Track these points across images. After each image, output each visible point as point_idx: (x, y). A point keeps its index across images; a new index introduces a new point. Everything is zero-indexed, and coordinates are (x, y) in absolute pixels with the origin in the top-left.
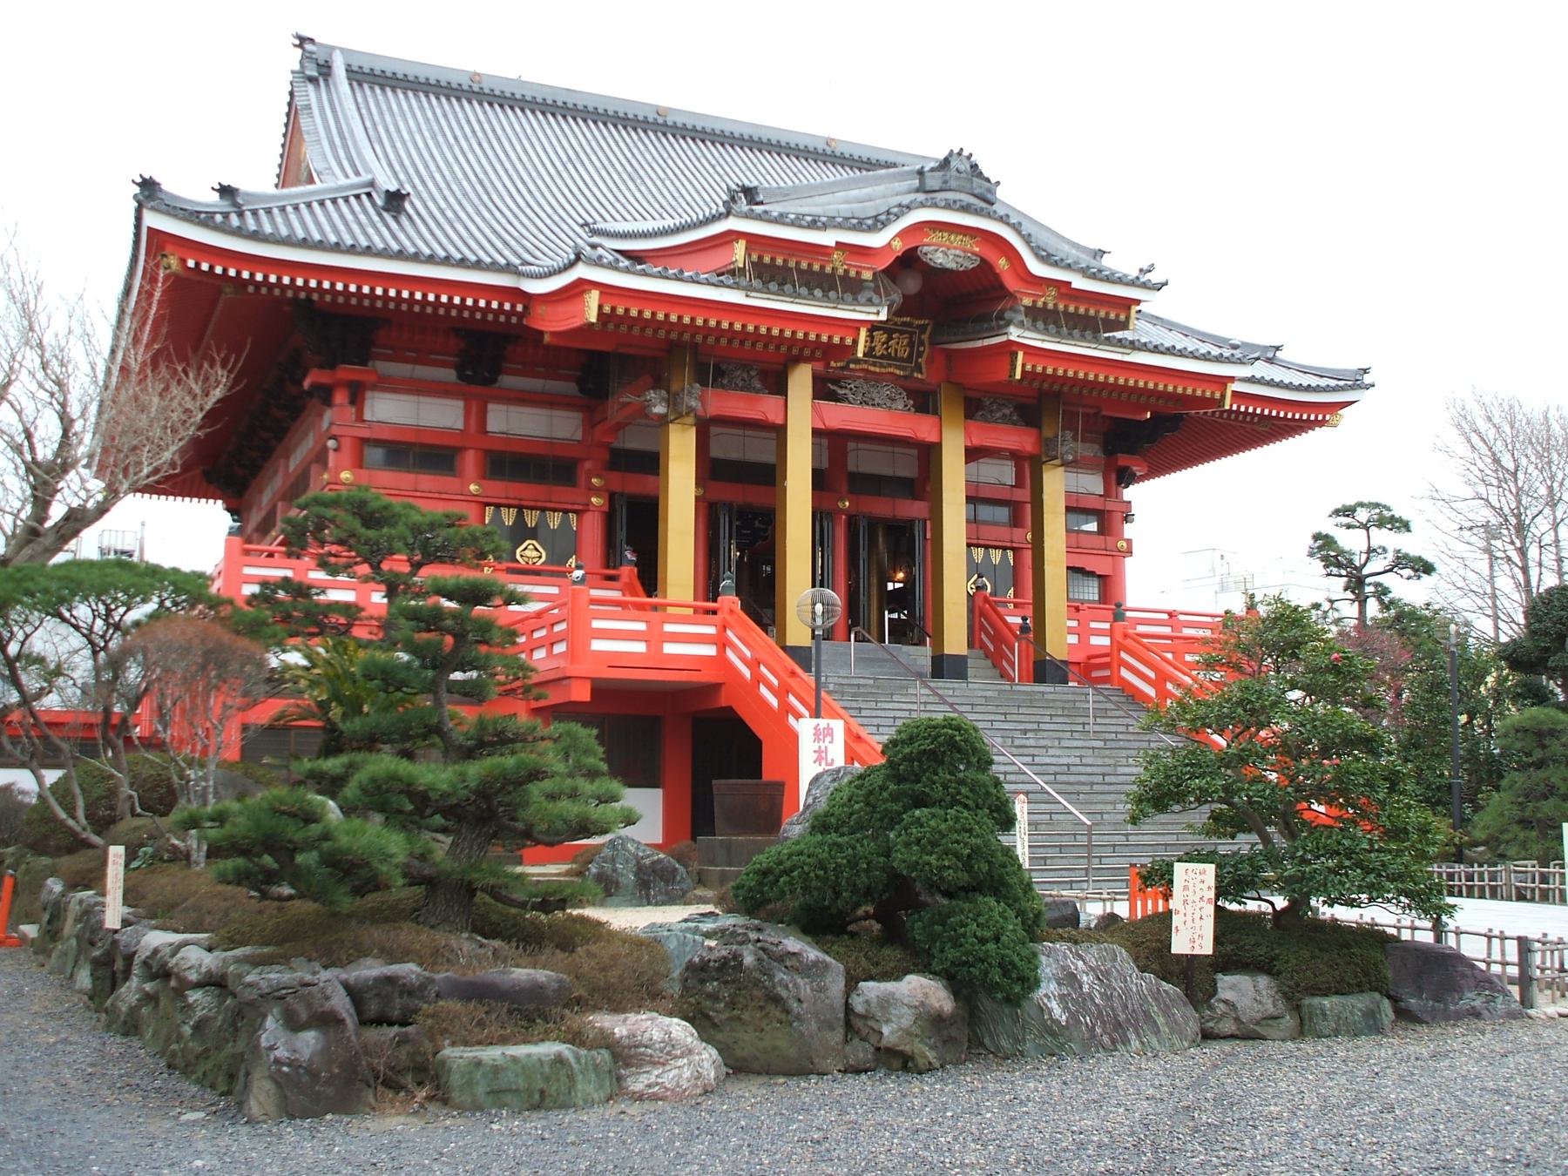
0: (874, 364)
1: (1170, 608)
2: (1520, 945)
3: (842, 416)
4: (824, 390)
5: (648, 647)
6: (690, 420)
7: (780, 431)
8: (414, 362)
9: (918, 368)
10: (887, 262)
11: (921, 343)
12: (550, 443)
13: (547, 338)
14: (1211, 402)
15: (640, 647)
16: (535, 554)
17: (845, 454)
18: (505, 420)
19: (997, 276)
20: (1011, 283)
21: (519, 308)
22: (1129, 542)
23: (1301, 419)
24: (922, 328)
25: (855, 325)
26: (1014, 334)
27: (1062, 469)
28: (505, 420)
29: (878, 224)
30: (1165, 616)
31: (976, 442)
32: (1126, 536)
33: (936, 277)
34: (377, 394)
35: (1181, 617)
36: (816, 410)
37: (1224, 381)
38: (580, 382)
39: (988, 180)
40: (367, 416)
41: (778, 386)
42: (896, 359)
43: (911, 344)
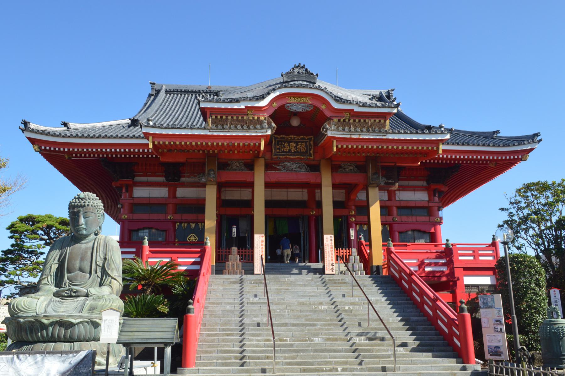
3: (276, 176)
4: (269, 167)
6: (215, 183)
9: (310, 155)
10: (271, 112)
11: (310, 145)
14: (426, 153)
16: (194, 238)
20: (328, 114)
22: (441, 218)
24: (310, 139)
25: (258, 138)
26: (329, 133)
28: (182, 193)
29: (262, 97)
32: (440, 216)
35: (457, 246)
37: (437, 142)
39: (312, 74)
41: (250, 166)
42: (301, 152)
43: (306, 146)
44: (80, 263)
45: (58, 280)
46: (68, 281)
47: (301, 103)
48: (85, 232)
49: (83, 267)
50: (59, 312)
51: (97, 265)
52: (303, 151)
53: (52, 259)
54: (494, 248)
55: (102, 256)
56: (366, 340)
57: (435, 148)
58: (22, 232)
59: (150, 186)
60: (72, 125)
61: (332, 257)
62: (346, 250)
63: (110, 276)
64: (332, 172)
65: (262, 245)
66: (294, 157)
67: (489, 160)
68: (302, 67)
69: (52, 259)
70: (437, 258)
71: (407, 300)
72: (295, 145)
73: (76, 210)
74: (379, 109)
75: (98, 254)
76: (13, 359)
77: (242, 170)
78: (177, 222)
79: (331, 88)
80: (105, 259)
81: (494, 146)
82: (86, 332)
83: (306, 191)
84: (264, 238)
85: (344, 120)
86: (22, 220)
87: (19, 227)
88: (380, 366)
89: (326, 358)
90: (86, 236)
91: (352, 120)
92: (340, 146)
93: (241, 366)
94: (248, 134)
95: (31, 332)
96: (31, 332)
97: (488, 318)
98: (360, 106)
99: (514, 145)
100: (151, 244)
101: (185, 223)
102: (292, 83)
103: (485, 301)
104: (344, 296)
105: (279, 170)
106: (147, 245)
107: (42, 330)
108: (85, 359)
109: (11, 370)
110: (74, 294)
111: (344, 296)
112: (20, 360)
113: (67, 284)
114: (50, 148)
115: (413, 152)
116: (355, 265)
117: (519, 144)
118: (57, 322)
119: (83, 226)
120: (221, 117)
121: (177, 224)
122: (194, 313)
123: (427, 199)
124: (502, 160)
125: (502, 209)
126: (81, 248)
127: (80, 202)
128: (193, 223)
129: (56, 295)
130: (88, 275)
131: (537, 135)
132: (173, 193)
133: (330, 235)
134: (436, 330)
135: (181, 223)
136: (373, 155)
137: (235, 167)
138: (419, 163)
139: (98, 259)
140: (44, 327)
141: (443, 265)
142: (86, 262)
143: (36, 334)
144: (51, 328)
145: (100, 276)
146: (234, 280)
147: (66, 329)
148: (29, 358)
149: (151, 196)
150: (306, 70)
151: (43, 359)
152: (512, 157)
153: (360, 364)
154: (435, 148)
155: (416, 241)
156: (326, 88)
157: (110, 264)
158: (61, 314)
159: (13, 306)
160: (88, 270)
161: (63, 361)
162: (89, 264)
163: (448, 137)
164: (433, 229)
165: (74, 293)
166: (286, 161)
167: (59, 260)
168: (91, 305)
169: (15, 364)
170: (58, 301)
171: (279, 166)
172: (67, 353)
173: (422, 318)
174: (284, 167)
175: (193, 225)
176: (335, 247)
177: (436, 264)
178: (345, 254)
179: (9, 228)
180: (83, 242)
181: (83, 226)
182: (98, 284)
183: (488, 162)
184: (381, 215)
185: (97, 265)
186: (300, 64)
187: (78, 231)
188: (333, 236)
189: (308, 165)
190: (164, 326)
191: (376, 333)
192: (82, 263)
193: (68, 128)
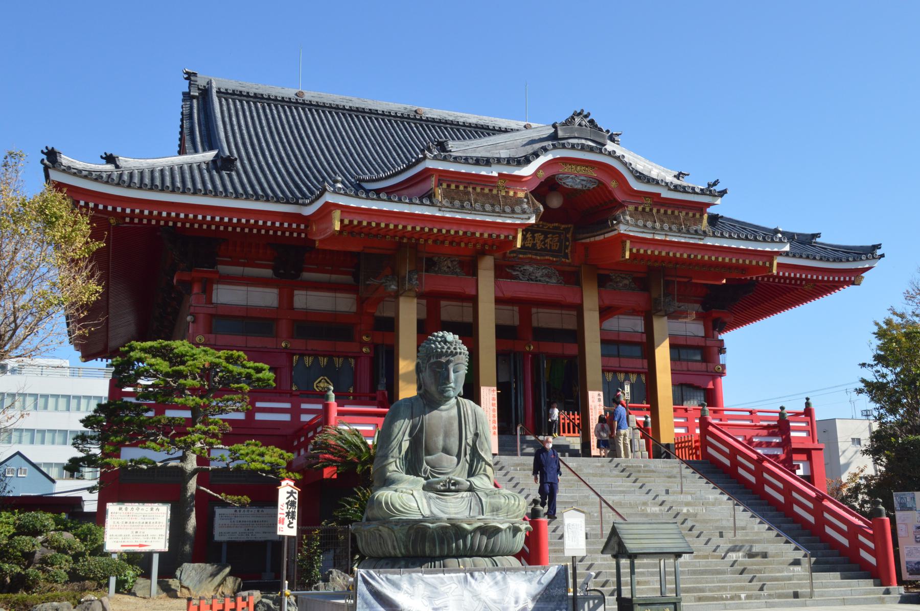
0: (536, 254)
1: (750, 408)
2: (122, 498)
4: (501, 272)
5: (292, 417)
6: (413, 294)
7: (474, 300)
8: (244, 265)
9: (566, 256)
10: (534, 186)
11: (567, 240)
12: (335, 315)
13: (317, 244)
15: (286, 417)
17: (530, 315)
18: (304, 300)
19: (610, 192)
20: (620, 196)
21: (302, 226)
22: (724, 366)
23: (839, 281)
24: (567, 230)
25: (514, 227)
26: (623, 229)
27: (666, 318)
28: (304, 300)
29: (527, 160)
30: (748, 413)
31: (607, 302)
33: (570, 195)
34: (220, 286)
35: (759, 414)
36: (497, 285)
37: (771, 255)
38: (275, 269)
39: (601, 130)
40: (214, 300)
41: (472, 270)
44: (445, 441)
46: (429, 468)
47: (581, 175)
49: (449, 446)
51: (467, 444)
52: (554, 248)
54: (808, 419)
55: (472, 429)
56: (744, 557)
57: (768, 264)
59: (247, 285)
60: (123, 161)
62: (573, 414)
63: (484, 460)
64: (599, 286)
65: (493, 405)
67: (806, 279)
68: (586, 116)
70: (770, 435)
71: (756, 499)
72: (542, 237)
73: (443, 360)
74: (696, 196)
76: (466, 578)
77: (456, 273)
78: (294, 354)
79: (629, 157)
81: (821, 259)
83: (516, 308)
85: (644, 209)
88: (791, 591)
89: (713, 582)
90: (449, 398)
91: (655, 211)
92: (634, 251)
94: (499, 220)
95: (442, 543)
96: (442, 543)
97: (906, 524)
98: (670, 189)
99: (848, 261)
100: (340, 400)
101: (309, 355)
102: (571, 141)
103: (903, 501)
104: (667, 492)
106: (333, 400)
107: (457, 540)
109: (466, 593)
110: (453, 488)
111: (667, 492)
114: (105, 207)
115: (716, 265)
117: (854, 260)
118: (479, 528)
120: (457, 187)
121: (295, 358)
123: (702, 333)
124: (823, 280)
125: (863, 365)
127: (449, 348)
128: (324, 356)
130: (455, 459)
131: (878, 247)
132: (287, 300)
133: (597, 392)
134: (822, 541)
135: (302, 355)
136: (656, 264)
137: (445, 268)
138: (724, 281)
139: (468, 433)
141: (778, 445)
142: (452, 439)
143: (449, 545)
150: (592, 122)
151: (504, 578)
152: (837, 279)
153: (761, 589)
154: (768, 264)
155: (685, 403)
156: (623, 156)
158: (452, 516)
159: (387, 504)
160: (456, 450)
161: (530, 581)
162: (457, 443)
163: (787, 248)
164: (711, 383)
165: (454, 484)
166: (526, 263)
167: (410, 435)
168: (490, 504)
169: (470, 586)
171: (515, 270)
173: (795, 526)
174: (524, 272)
175: (324, 361)
177: (769, 445)
178: (567, 421)
180: (442, 407)
183: (804, 283)
184: (672, 359)
186: (582, 111)
188: (601, 393)
189: (562, 273)
191: (751, 546)
193: (117, 167)
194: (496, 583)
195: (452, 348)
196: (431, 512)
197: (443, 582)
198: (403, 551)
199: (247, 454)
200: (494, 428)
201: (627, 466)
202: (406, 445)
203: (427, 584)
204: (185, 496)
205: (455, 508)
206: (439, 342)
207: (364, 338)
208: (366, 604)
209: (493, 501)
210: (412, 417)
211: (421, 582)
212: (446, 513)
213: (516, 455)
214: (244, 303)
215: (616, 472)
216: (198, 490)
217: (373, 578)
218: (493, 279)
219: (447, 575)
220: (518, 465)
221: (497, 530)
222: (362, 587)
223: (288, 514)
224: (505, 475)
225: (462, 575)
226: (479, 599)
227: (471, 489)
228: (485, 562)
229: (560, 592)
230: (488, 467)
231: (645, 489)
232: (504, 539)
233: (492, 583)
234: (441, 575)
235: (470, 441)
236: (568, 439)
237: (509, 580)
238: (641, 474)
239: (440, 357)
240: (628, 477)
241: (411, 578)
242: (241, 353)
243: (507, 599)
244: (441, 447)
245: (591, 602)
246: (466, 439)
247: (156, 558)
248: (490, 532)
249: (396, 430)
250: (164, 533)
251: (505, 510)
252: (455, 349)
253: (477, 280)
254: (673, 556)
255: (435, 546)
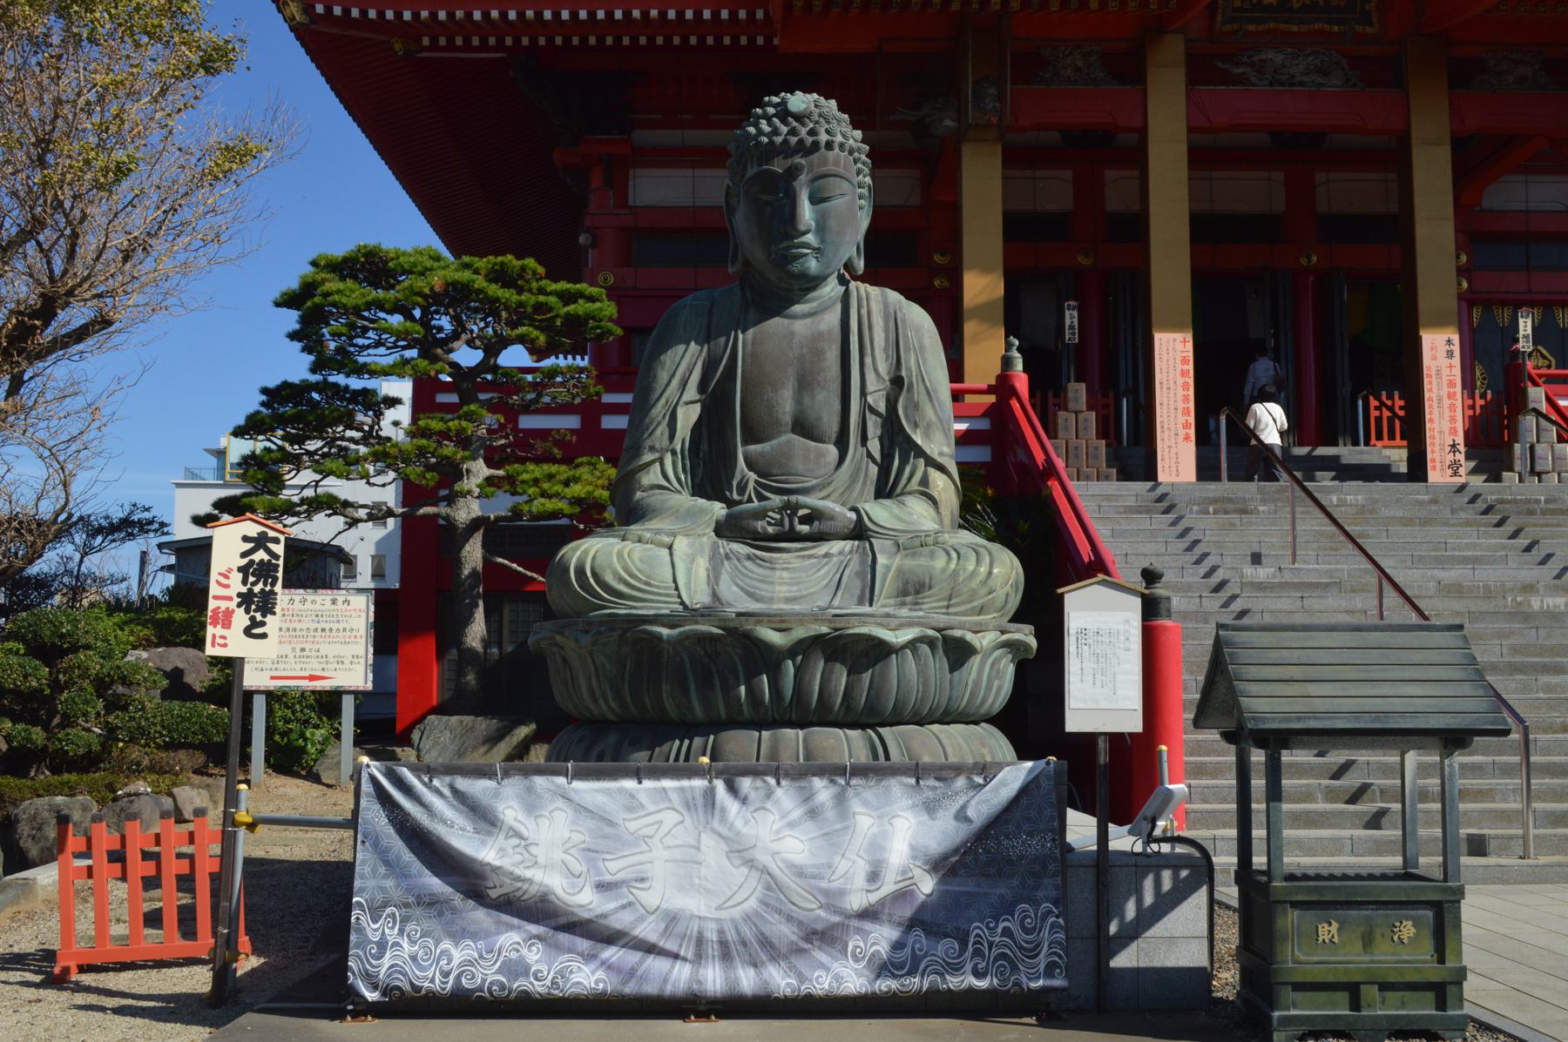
4: (1200, 71)
34: (640, 172)
41: (1130, 70)
44: (798, 401)
45: (700, 471)
46: (752, 476)
48: (813, 265)
50: (771, 600)
51: (867, 408)
53: (675, 382)
55: (884, 368)
58: (357, 311)
61: (1453, 419)
63: (920, 453)
66: (1304, 28)
69: (675, 382)
73: (778, 167)
75: (868, 360)
76: (710, 794)
80: (897, 382)
82: (926, 684)
83: (1278, 176)
84: (1190, 346)
86: (344, 267)
87: (339, 291)
90: (816, 282)
93: (1368, 826)
105: (1240, 80)
108: (1025, 800)
109: (708, 840)
110: (805, 528)
112: (744, 801)
113: (751, 485)
116: (1539, 449)
118: (817, 640)
119: (810, 238)
122: (1169, 616)
126: (793, 334)
127: (793, 132)
129: (725, 530)
130: (832, 451)
139: (870, 377)
140: (761, 658)
142: (821, 396)
144: (790, 668)
145: (877, 456)
146: (1131, 502)
147: (854, 671)
148: (779, 792)
149: (699, 203)
151: (840, 799)
157: (916, 406)
159: (580, 571)
160: (831, 424)
161: (930, 808)
162: (837, 405)
165: (805, 520)
167: (702, 387)
168: (900, 571)
170: (749, 557)
172: (945, 772)
176: (1464, 387)
179: (289, 301)
181: (810, 238)
182: (871, 489)
185: (867, 408)
187: (787, 259)
188: (1456, 338)
190: (1418, 657)
192: (807, 400)
194: (813, 814)
195: (803, 131)
196: (715, 595)
197: (632, 805)
198: (614, 705)
199: (536, 482)
200: (1186, 425)
201: (1501, 502)
202: (688, 416)
203: (581, 809)
204: (459, 575)
205: (796, 589)
206: (769, 119)
207: (937, 258)
208: (387, 863)
209: (910, 563)
210: (706, 338)
211: (560, 803)
212: (758, 599)
213: (1218, 478)
214: (688, 202)
215: (1469, 514)
216: (487, 562)
217: (407, 790)
218: (1182, 88)
219: (648, 784)
220: (1215, 501)
221: (878, 651)
222: (374, 815)
223: (246, 600)
224: (1174, 524)
225: (699, 783)
226: (751, 863)
227: (859, 532)
228: (849, 744)
229: (1037, 846)
230: (934, 474)
231: (1537, 554)
232: (912, 676)
233: (797, 813)
234: (630, 784)
235: (878, 401)
236: (1387, 452)
237: (856, 806)
238: (1532, 519)
239: (769, 160)
240: (1500, 524)
241: (530, 790)
242: (530, 262)
243: (843, 866)
244: (787, 419)
245: (1167, 875)
246: (863, 394)
247: (348, 705)
248: (867, 653)
249: (663, 376)
250: (362, 653)
251: (941, 589)
252: (812, 132)
253: (1145, 92)
254: (1434, 740)
255: (686, 692)
